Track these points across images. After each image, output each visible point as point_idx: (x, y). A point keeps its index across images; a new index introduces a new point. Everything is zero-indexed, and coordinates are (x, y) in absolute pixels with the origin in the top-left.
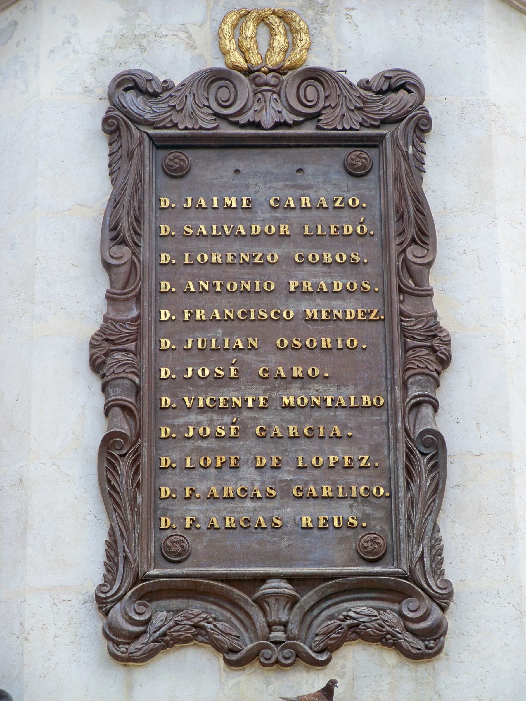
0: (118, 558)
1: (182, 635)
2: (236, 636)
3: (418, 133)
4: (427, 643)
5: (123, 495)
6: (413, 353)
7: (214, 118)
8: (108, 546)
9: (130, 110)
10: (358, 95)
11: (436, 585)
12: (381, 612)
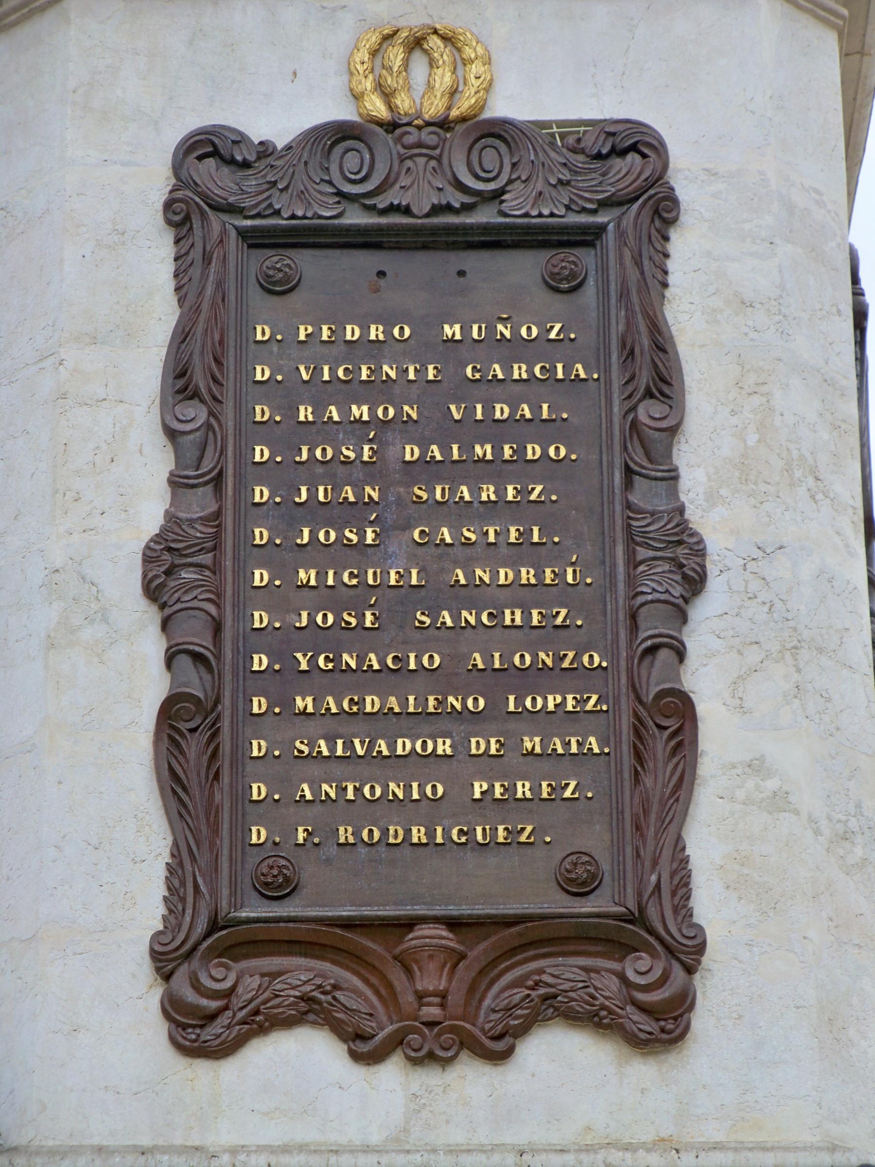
0: (185, 890)
1: (284, 1012)
3: (657, 223)
4: (662, 1023)
5: (195, 797)
6: (646, 568)
7: (337, 199)
8: (170, 872)
12: (593, 975)
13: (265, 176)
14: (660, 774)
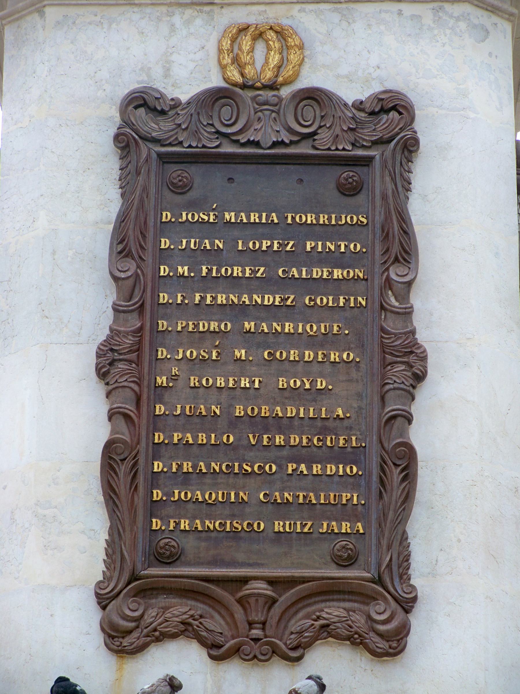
2: (218, 633)
3: (406, 153)
7: (217, 136)
9: (138, 127)
11: (402, 588)
12: (351, 613)
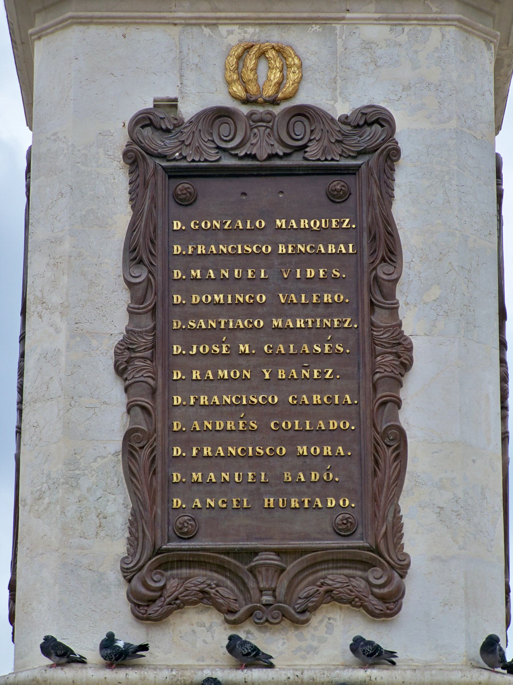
1: (190, 599)
3: (389, 162)
4: (387, 605)
7: (217, 151)
10: (338, 129)
12: (351, 579)
13: (177, 138)
14: (387, 471)
